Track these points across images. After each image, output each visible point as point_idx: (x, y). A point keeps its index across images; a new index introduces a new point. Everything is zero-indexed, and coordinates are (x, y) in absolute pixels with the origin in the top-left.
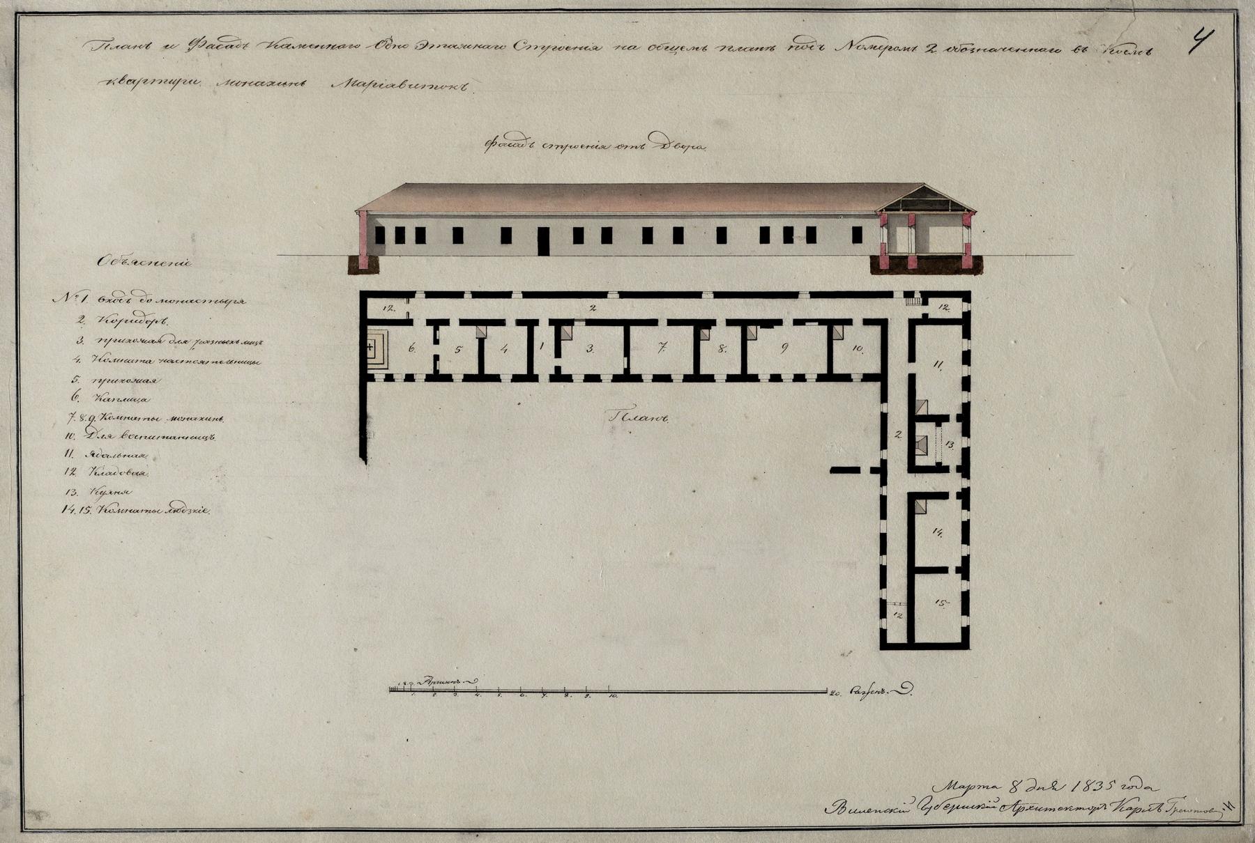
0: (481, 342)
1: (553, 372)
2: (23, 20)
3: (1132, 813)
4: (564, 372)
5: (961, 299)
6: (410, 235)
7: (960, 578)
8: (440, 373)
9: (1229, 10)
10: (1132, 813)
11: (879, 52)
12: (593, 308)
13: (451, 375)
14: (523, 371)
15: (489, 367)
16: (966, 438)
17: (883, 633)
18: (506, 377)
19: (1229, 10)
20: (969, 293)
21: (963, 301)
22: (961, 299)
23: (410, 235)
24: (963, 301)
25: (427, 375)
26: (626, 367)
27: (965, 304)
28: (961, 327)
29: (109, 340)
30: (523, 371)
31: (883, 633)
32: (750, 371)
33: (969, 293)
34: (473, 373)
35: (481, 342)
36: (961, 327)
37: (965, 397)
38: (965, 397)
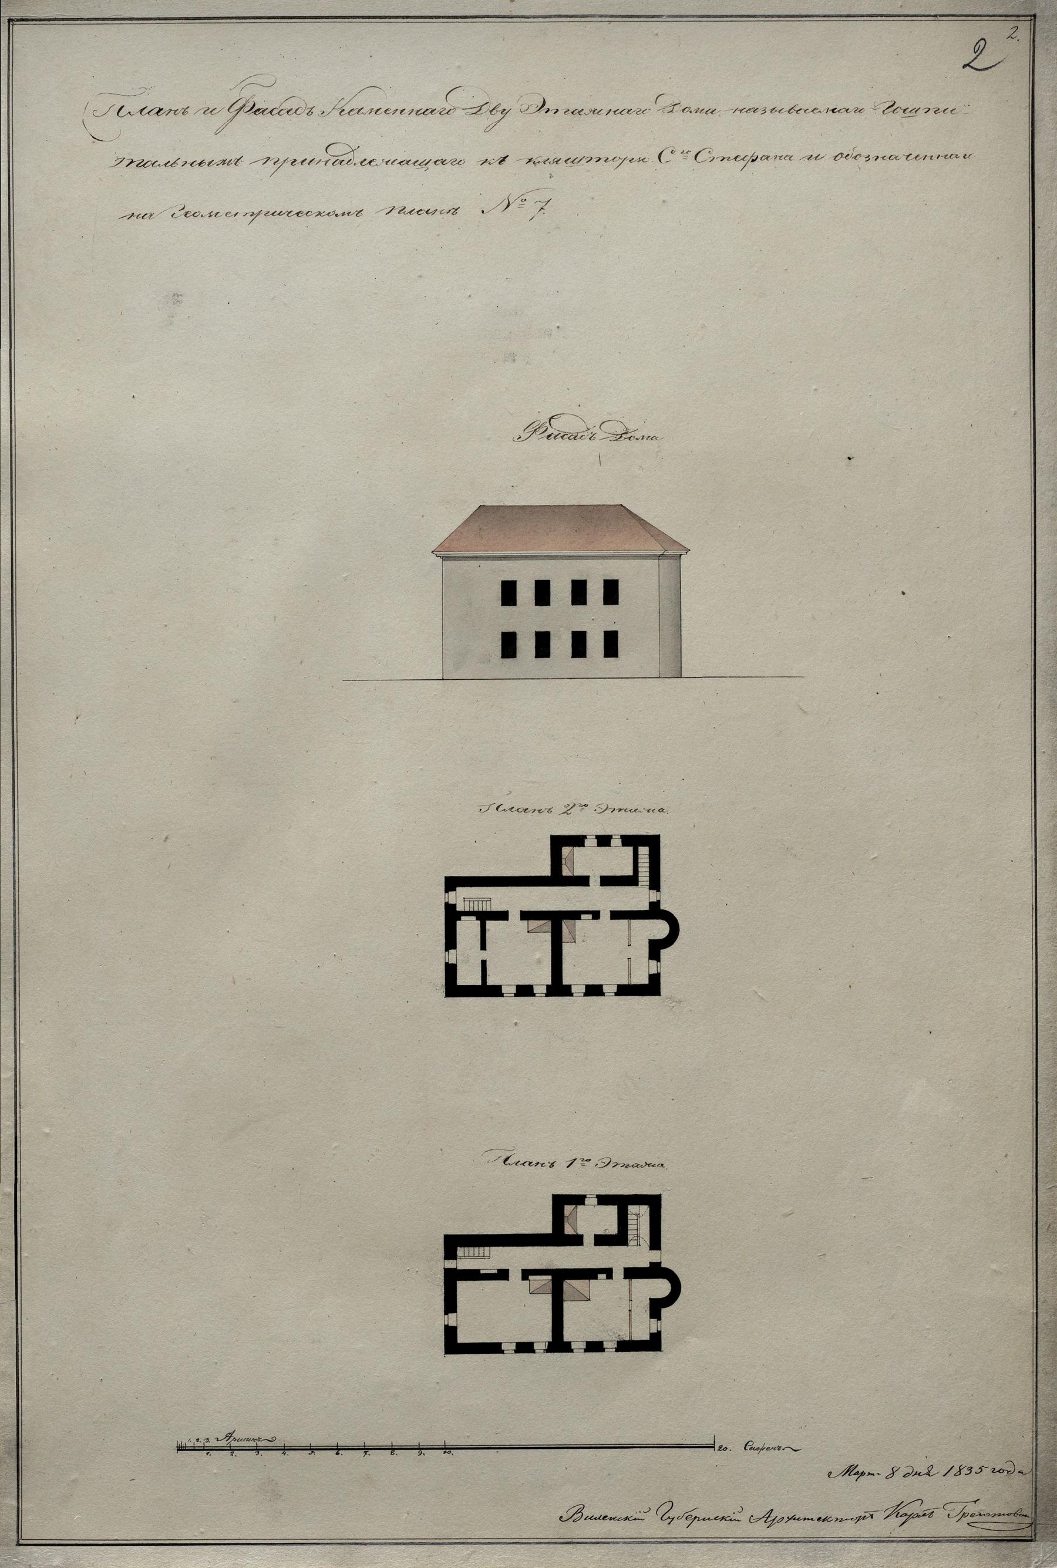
0: (630, 974)
3: (858, 1478)
5: (550, 983)
6: (595, 644)
10: (858, 1478)
11: (743, 163)
12: (4, 31)
17: (451, 970)
21: (548, 986)
22: (550, 983)
23: (595, 644)
24: (548, 986)
28: (488, 922)
29: (281, 160)
31: (451, 970)
34: (544, 874)
35: (630, 974)
36: (488, 922)
37: (509, 989)
38: (509, 989)
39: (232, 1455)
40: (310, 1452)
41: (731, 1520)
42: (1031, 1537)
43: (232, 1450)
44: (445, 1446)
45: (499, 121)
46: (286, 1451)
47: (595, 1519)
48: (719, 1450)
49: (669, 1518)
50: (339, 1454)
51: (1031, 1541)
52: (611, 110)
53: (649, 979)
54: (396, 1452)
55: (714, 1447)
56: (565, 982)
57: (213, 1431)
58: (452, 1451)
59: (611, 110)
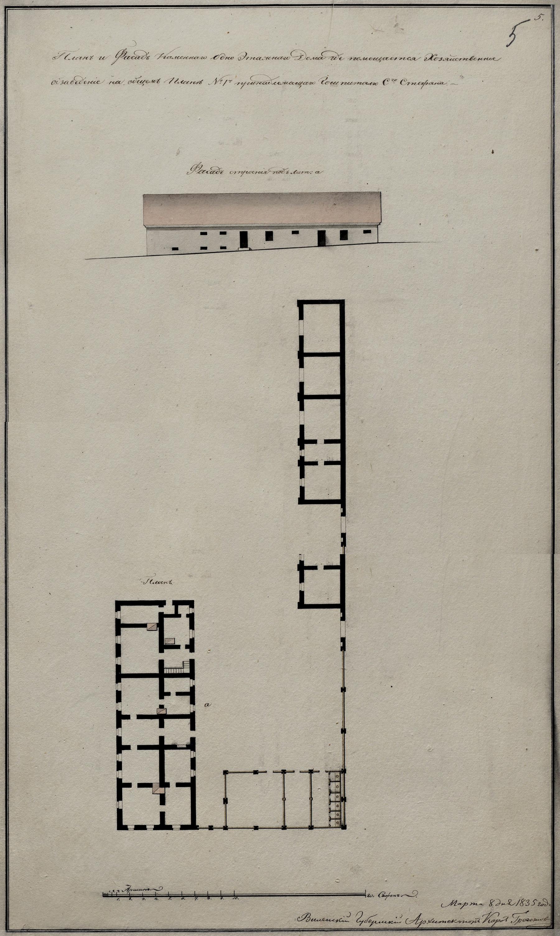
1: (188, 650)
2: (336, 308)
4: (188, 643)
7: (122, 712)
8: (339, 609)
9: (13, 931)
13: (304, 477)
14: (188, 822)
15: (437, 2)
16: (119, 710)
18: (120, 774)
19: (13, 931)
20: (193, 601)
21: (190, 607)
25: (303, 561)
26: (178, 747)
27: (191, 609)
30: (188, 822)
32: (123, 630)
33: (193, 601)
39: (130, 899)
40: (168, 898)
41: (343, 921)
42: (9, 930)
43: (130, 897)
44: (182, 894)
45: (61, 56)
46: (157, 898)
47: (317, 921)
48: (368, 897)
49: (360, 921)
50: (222, 898)
51: (6, 929)
52: (111, 82)
53: (190, 689)
54: (224, 898)
55: (365, 895)
56: (122, 680)
57: (121, 888)
58: (238, 897)
59: (111, 82)
